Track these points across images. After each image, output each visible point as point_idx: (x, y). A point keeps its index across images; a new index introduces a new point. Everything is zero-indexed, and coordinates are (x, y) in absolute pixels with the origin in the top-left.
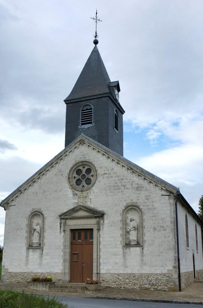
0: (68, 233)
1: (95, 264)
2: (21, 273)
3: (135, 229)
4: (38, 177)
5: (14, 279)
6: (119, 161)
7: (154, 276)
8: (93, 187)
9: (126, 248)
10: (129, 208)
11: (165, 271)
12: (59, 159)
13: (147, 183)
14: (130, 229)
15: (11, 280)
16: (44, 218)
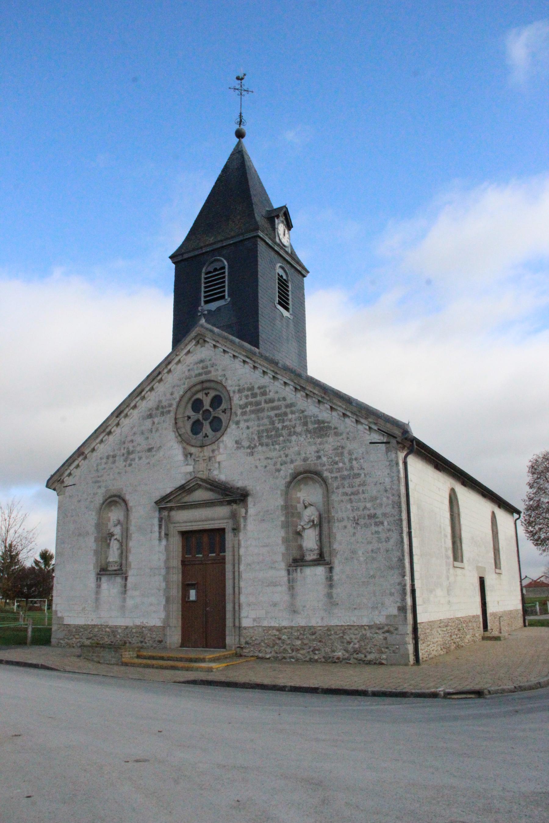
0: (176, 542)
1: (229, 607)
2: (85, 627)
3: (314, 525)
4: (117, 422)
5: (74, 640)
6: (276, 373)
7: (356, 632)
8: (225, 435)
9: (294, 568)
10: (299, 477)
11: (380, 619)
12: (155, 381)
13: (338, 417)
14: (302, 526)
15: (69, 641)
16: (128, 510)
